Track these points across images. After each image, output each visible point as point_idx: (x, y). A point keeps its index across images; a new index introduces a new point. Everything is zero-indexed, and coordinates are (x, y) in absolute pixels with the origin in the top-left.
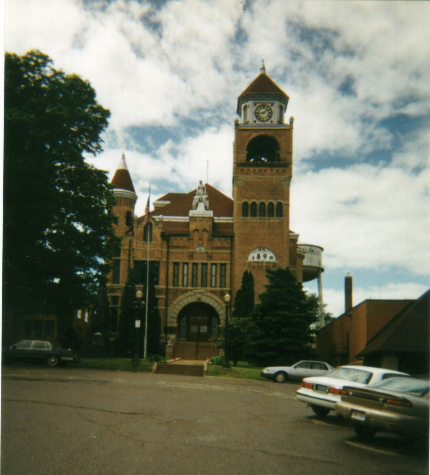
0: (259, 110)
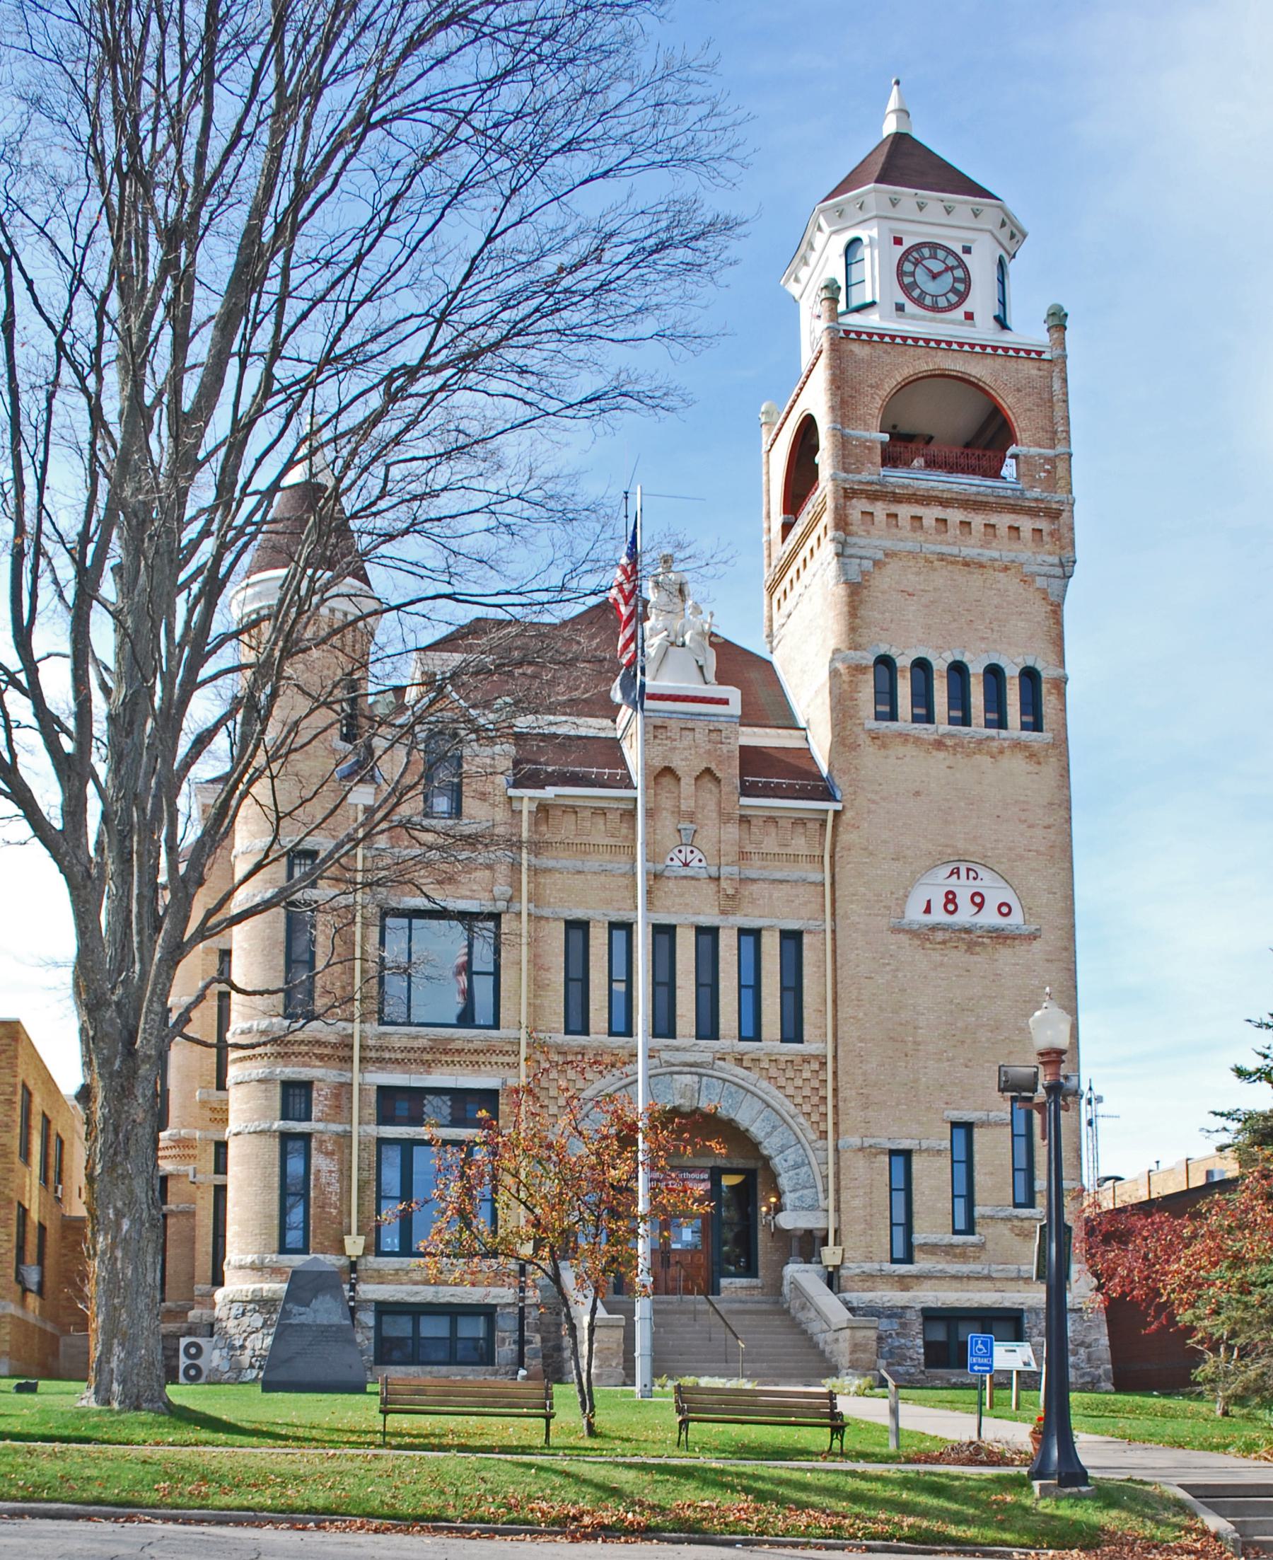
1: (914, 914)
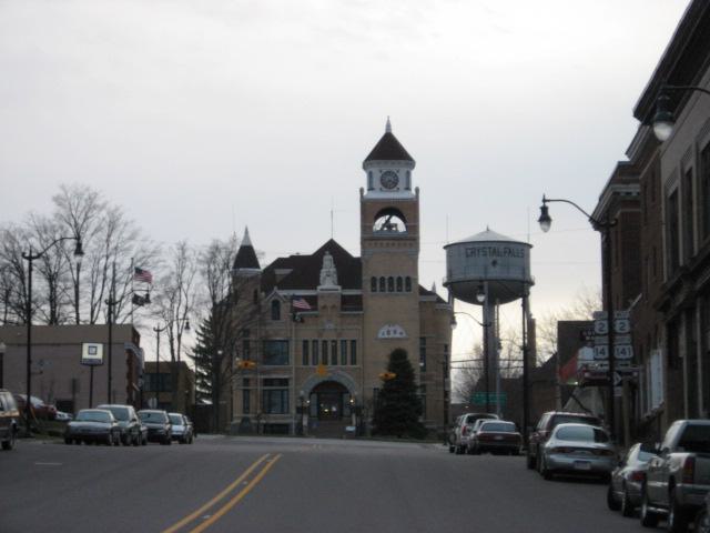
1: (380, 336)
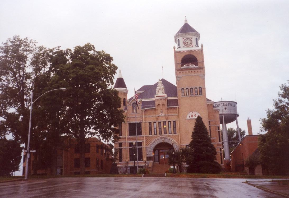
0: (185, 41)
1: (188, 118)
